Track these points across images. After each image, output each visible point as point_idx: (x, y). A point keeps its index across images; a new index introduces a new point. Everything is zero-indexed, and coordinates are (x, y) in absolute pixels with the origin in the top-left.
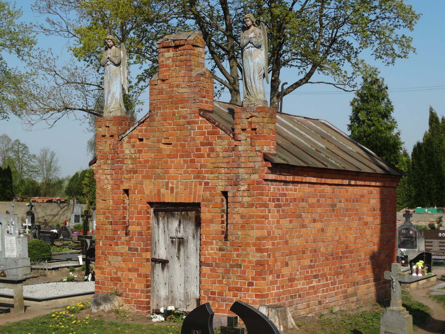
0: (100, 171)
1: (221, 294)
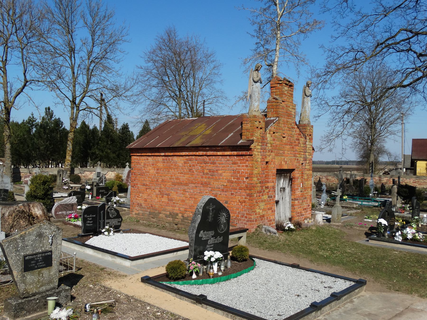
0: (255, 150)
1: (301, 213)
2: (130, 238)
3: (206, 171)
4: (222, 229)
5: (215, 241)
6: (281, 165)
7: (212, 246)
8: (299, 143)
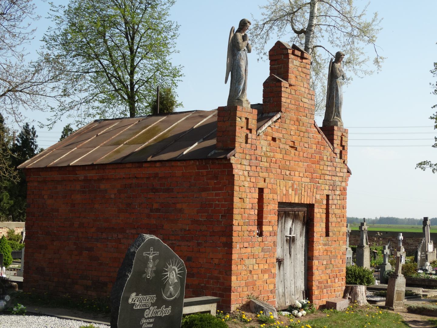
2: (13, 320)
3: (155, 206)
4: (171, 294)
5: (157, 313)
6: (287, 195)
7: (152, 320)
8: (321, 159)
